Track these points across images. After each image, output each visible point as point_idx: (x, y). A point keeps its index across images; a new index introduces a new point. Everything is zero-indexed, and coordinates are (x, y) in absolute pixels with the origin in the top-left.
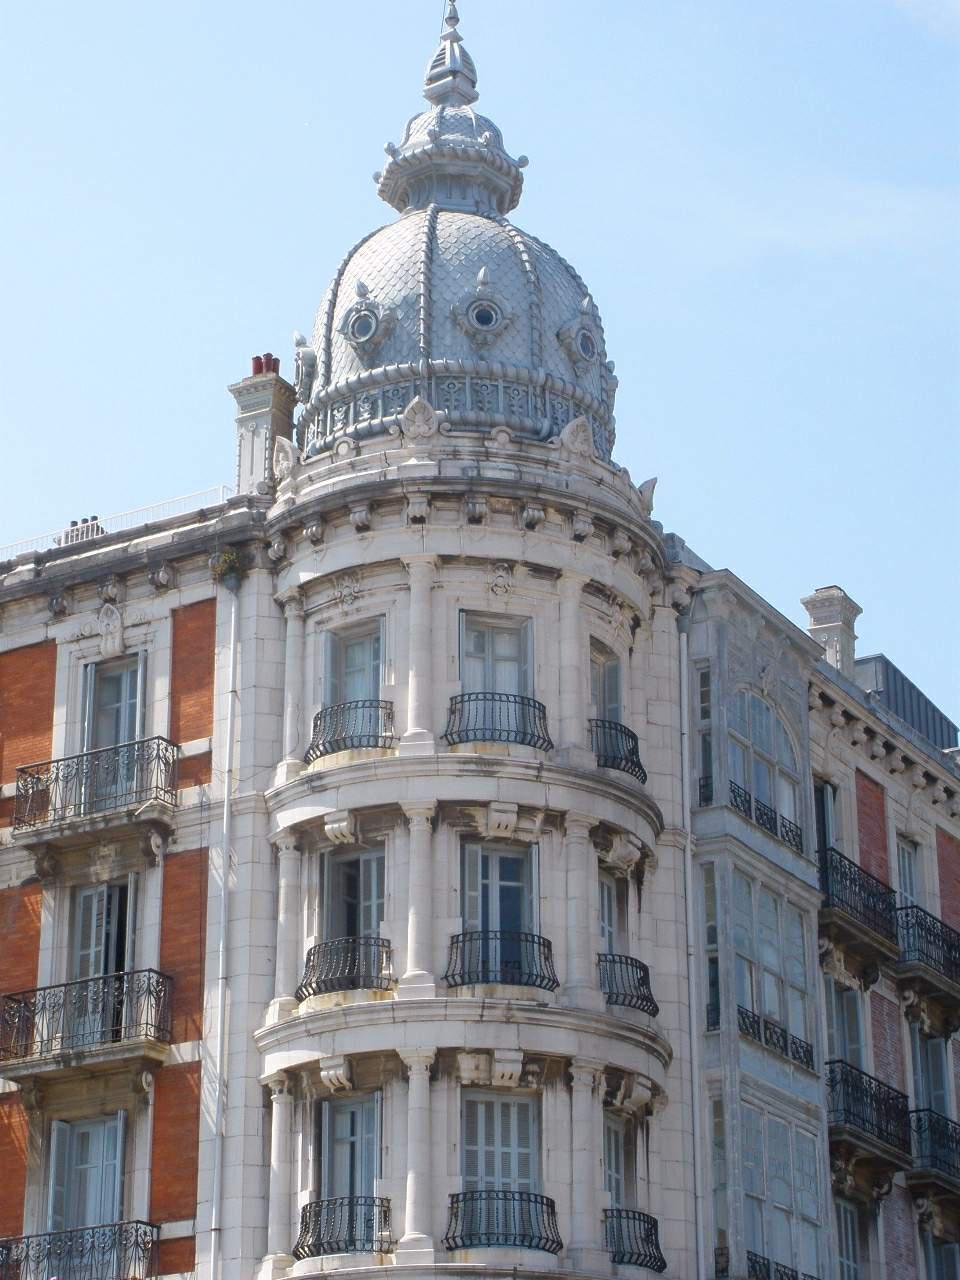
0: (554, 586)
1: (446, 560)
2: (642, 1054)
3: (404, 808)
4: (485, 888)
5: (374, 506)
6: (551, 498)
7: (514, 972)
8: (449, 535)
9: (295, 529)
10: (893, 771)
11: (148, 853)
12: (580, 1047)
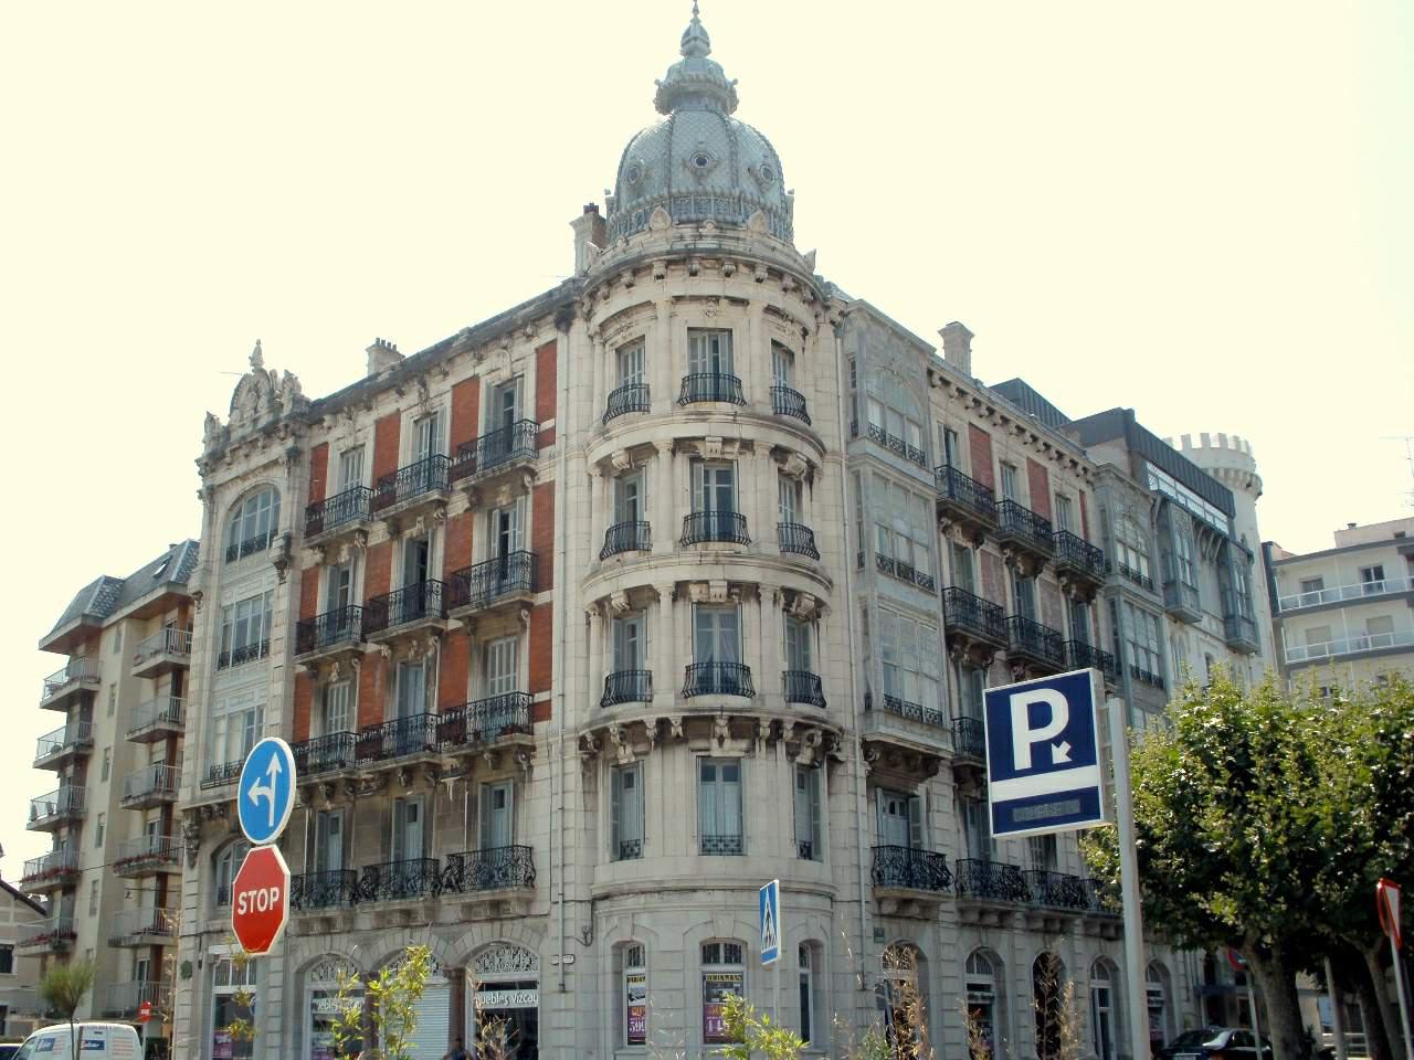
0: (745, 310)
1: (678, 299)
2: (808, 581)
3: (655, 444)
4: (707, 490)
5: (635, 272)
6: (739, 257)
7: (726, 535)
8: (678, 284)
9: (596, 292)
10: (995, 425)
11: (524, 486)
12: (764, 577)
